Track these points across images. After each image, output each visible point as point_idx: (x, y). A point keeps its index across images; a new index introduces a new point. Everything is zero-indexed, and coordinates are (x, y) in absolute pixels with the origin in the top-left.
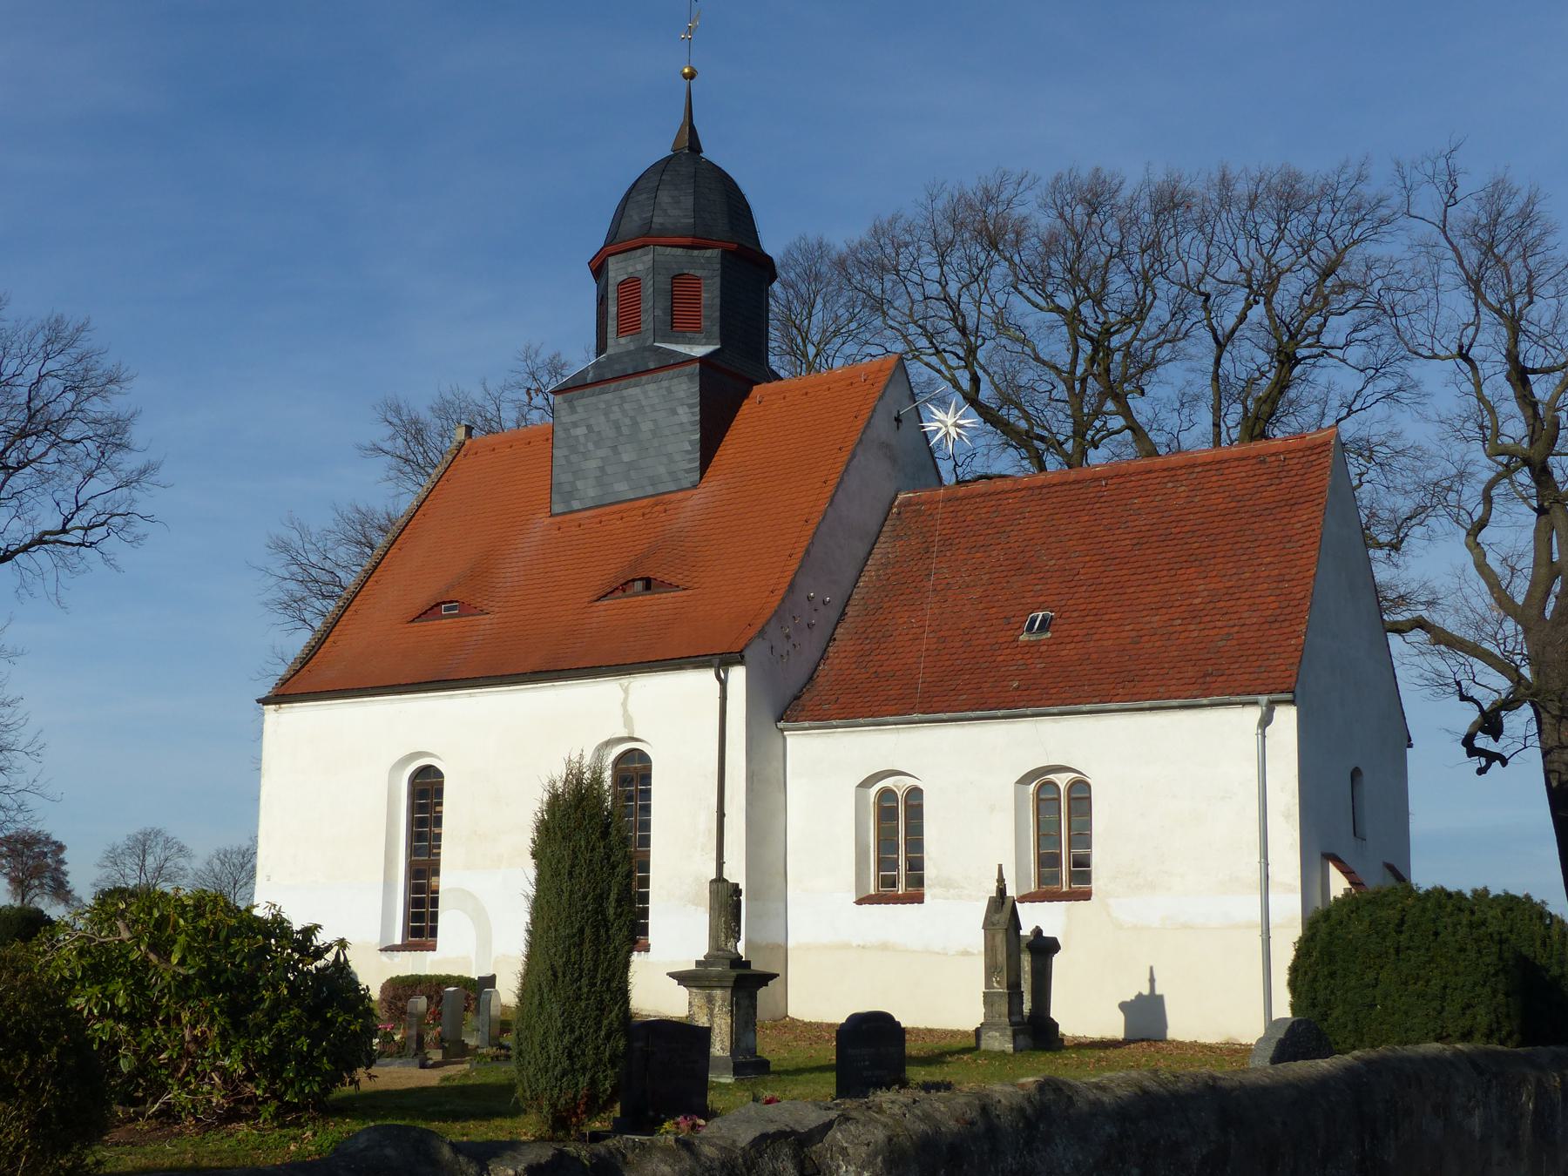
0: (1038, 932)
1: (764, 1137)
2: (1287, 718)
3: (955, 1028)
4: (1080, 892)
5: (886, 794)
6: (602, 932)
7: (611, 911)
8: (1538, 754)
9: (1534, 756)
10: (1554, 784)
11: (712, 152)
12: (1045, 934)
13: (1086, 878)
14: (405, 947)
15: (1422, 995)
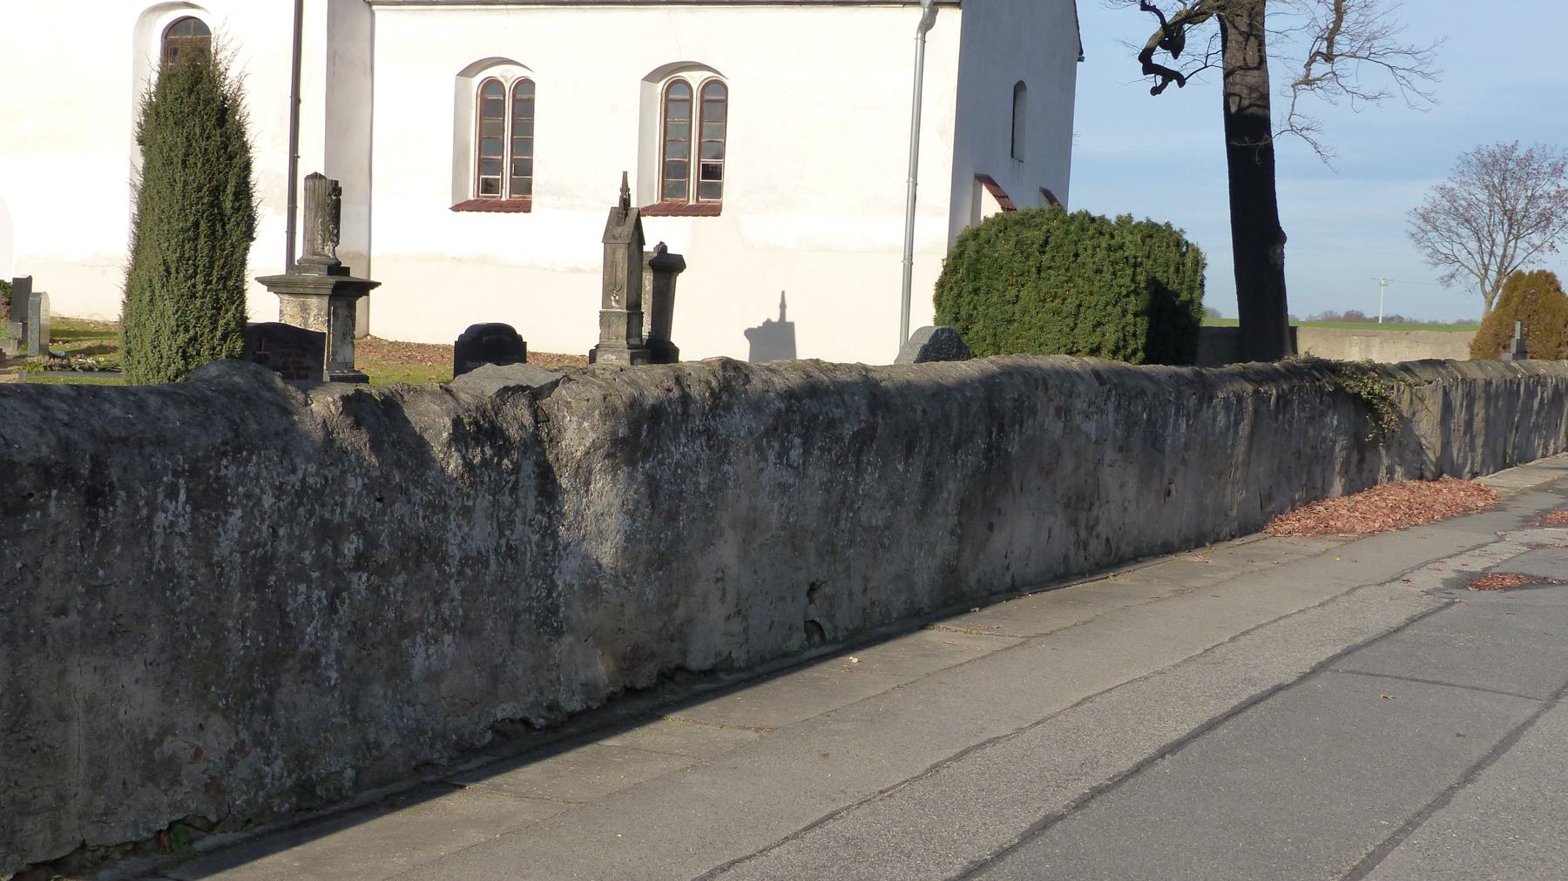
0: (662, 248)
1: (506, 389)
2: (950, 21)
3: (560, 352)
5: (492, 85)
6: (218, 227)
7: (228, 205)
8: (1220, 74)
9: (1216, 76)
10: (1233, 109)
12: (670, 251)
13: (717, 191)
15: (1056, 313)
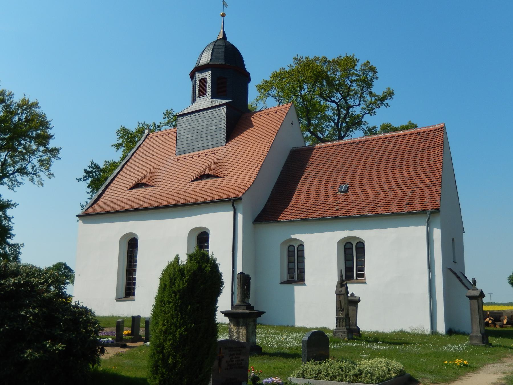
11: (229, 39)
14: (125, 297)
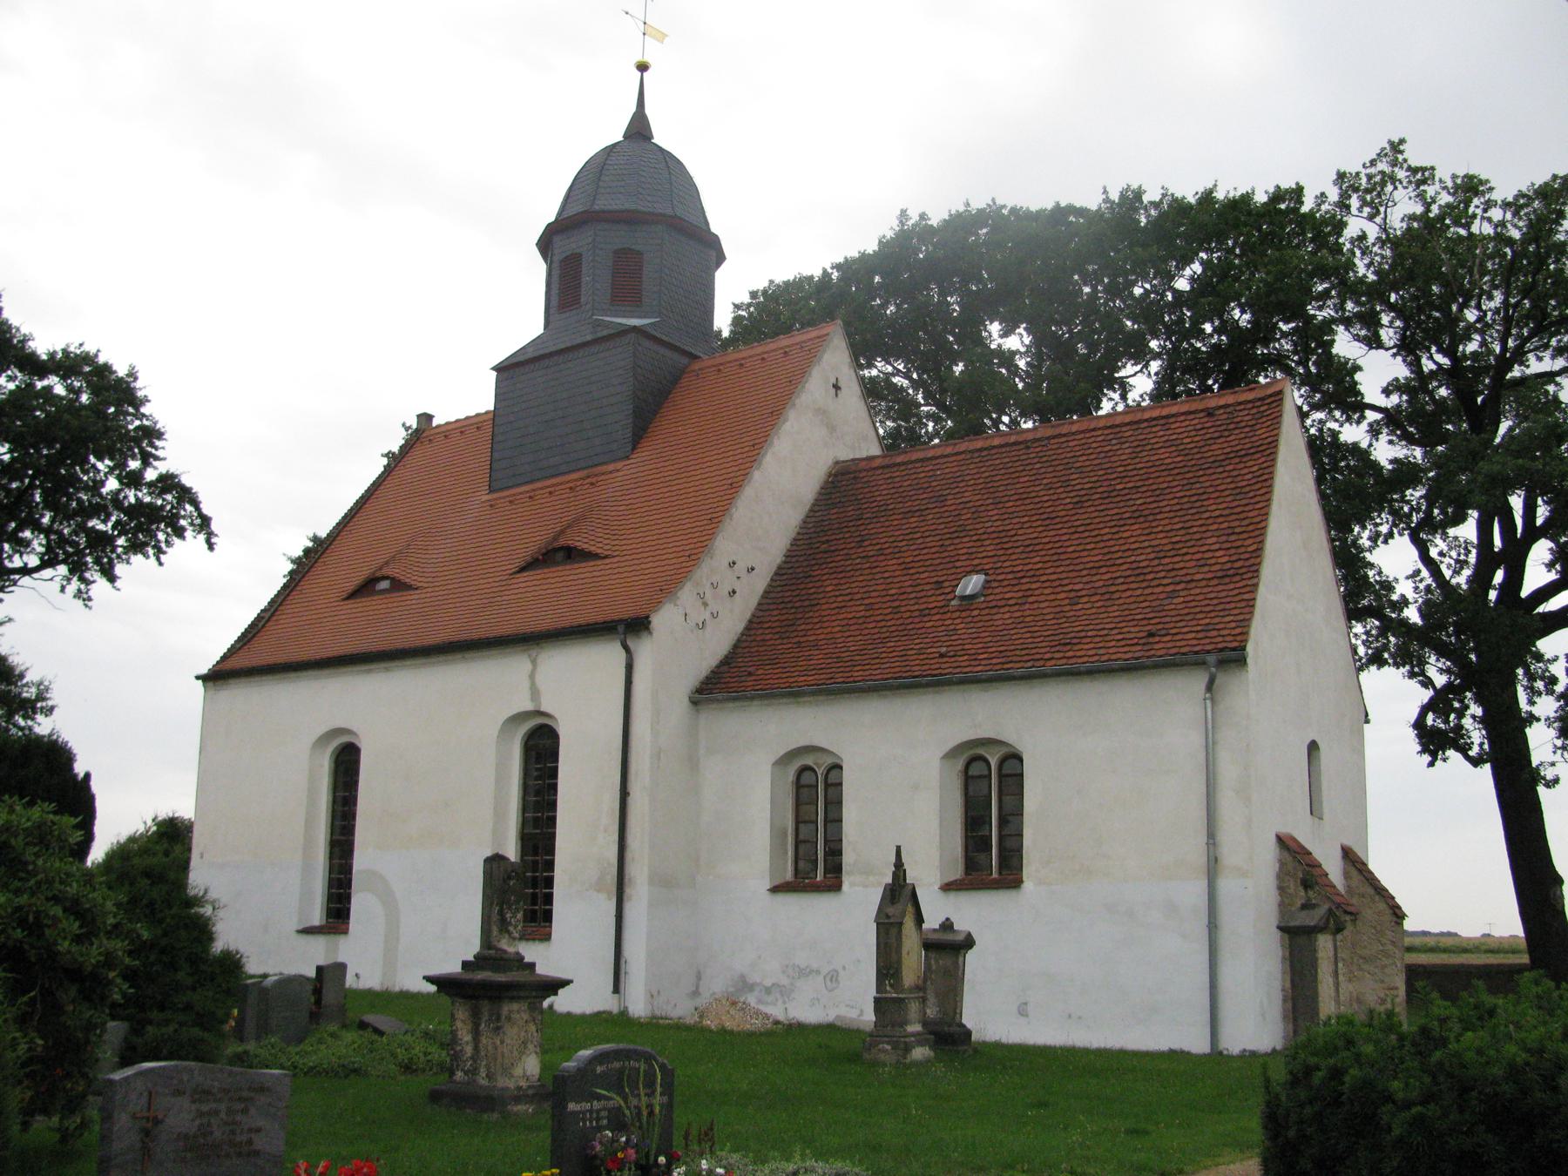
4: (1009, 875)
